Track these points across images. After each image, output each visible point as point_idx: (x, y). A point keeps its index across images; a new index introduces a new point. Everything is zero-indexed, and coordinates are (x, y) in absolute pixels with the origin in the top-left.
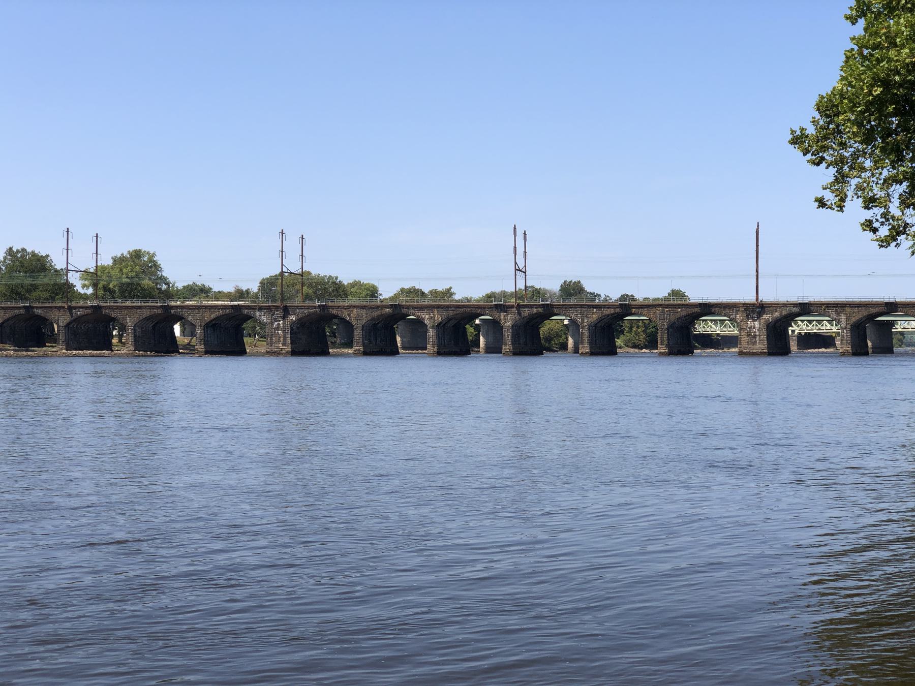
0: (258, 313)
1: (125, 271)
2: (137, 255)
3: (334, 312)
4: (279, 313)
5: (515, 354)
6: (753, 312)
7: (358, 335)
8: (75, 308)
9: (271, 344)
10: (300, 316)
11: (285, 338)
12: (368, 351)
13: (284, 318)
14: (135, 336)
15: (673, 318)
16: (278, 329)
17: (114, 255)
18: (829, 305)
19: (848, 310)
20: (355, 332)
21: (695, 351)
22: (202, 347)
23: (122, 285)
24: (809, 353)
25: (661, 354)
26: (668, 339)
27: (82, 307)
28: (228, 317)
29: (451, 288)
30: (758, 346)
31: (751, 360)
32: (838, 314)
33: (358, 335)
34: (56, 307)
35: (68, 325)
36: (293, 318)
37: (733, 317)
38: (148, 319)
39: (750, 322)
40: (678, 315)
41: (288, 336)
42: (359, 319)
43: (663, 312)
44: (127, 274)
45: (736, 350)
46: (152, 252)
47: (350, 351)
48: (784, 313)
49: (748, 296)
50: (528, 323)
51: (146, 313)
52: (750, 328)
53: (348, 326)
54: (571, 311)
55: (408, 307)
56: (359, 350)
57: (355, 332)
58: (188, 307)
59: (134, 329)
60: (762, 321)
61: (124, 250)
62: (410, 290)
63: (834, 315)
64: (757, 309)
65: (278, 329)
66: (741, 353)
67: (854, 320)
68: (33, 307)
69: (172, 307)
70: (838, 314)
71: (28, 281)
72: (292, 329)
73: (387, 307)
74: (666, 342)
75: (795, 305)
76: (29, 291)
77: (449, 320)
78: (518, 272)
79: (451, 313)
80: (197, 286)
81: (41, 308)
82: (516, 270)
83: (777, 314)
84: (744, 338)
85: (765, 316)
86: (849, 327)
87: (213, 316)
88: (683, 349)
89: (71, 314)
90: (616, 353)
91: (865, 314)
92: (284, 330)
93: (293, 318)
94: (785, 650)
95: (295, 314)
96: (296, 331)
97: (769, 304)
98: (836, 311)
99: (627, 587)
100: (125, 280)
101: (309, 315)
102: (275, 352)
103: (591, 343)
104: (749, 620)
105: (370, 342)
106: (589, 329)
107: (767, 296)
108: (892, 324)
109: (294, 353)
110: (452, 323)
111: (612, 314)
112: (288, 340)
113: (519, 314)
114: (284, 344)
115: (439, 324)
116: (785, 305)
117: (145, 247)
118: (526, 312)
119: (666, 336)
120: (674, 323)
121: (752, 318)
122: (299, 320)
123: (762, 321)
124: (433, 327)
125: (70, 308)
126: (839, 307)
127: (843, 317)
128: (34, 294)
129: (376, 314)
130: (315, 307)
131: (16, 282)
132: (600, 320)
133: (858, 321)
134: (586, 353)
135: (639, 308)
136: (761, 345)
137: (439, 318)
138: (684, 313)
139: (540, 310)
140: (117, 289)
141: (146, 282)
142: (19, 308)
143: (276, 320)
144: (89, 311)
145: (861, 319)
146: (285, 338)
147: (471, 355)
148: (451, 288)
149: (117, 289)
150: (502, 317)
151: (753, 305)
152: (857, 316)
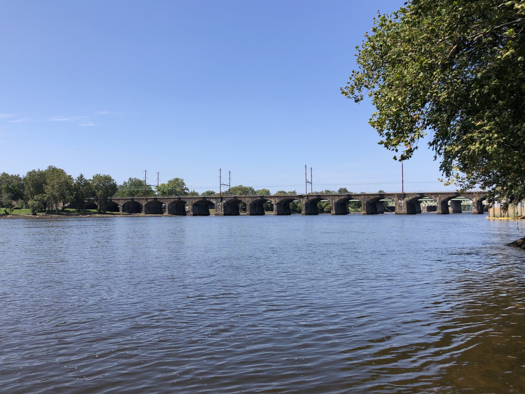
0: (212, 200)
1: (170, 185)
2: (177, 180)
3: (239, 199)
4: (219, 200)
5: (306, 214)
6: (401, 197)
7: (248, 207)
8: (148, 199)
9: (217, 211)
10: (227, 201)
11: (221, 210)
12: (252, 213)
13: (221, 201)
14: (169, 209)
15: (368, 200)
16: (219, 206)
17: (169, 180)
18: (432, 194)
19: (440, 195)
20: (247, 207)
21: (384, 213)
22: (192, 213)
23: (169, 191)
24: (431, 213)
25: (438, 214)
26: (367, 208)
27: (151, 199)
28: (259, 201)
29: (295, 191)
30: (403, 211)
31: (399, 216)
32: (436, 197)
33: (248, 207)
34: (193, 198)
35: (146, 205)
36: (224, 201)
37: (393, 199)
38: (174, 202)
39: (400, 201)
40: (371, 199)
41: (223, 208)
42: (248, 201)
43: (364, 197)
44: (170, 186)
45: (395, 212)
46: (182, 179)
47: (246, 214)
48: (414, 197)
49: (400, 191)
50: (312, 202)
51: (173, 200)
52: (400, 203)
53: (245, 205)
54: (328, 197)
55: (266, 197)
56: (248, 213)
57: (247, 206)
58: (187, 198)
59: (168, 206)
60: (405, 201)
61: (172, 178)
62: (281, 192)
63: (434, 197)
64: (402, 196)
65: (219, 206)
66: (396, 214)
67: (442, 199)
68: (134, 199)
69: (181, 198)
70: (436, 197)
71: (136, 189)
72: (224, 206)
73: (258, 197)
74: (365, 209)
75: (418, 194)
76: (136, 193)
77: (282, 201)
78: (307, 183)
79: (282, 199)
80: (210, 191)
81: (137, 199)
82: (306, 182)
83: (410, 198)
84: (397, 208)
85: (405, 199)
86: (440, 202)
87: (196, 201)
88: (373, 212)
89: (147, 201)
90: (421, 213)
91: (447, 197)
92: (221, 206)
93: (224, 201)
94: (176, 372)
95: (225, 200)
96: (225, 206)
97: (407, 194)
98: (435, 196)
99: (23, 336)
100: (170, 189)
101: (230, 200)
102: (218, 214)
103: (336, 210)
104: (165, 353)
105: (253, 210)
106: (335, 204)
107: (406, 191)
108: (461, 202)
109: (225, 215)
110: (283, 203)
111: (344, 199)
112: (223, 210)
113: (308, 199)
114: (221, 211)
115: (278, 203)
116: (414, 194)
117: (179, 177)
118: (310, 198)
119: (365, 207)
120: (369, 202)
121: (401, 199)
122: (227, 202)
123: (405, 201)
124: (275, 204)
125: (146, 199)
126: (436, 194)
127: (438, 198)
128: (138, 194)
129: (254, 200)
130: (232, 197)
131: (132, 190)
132: (340, 201)
133: (444, 200)
134: (334, 214)
135: (355, 196)
136: (404, 210)
137: (278, 201)
138: (373, 198)
139: (316, 197)
140: (167, 192)
141: (178, 189)
142: (129, 199)
143: (218, 202)
144: (153, 200)
145: (445, 199)
146: (221, 210)
147: (319, 215)
148: (295, 191)
149: (167, 192)
150: (301, 200)
151: (401, 194)
152: (444, 198)
